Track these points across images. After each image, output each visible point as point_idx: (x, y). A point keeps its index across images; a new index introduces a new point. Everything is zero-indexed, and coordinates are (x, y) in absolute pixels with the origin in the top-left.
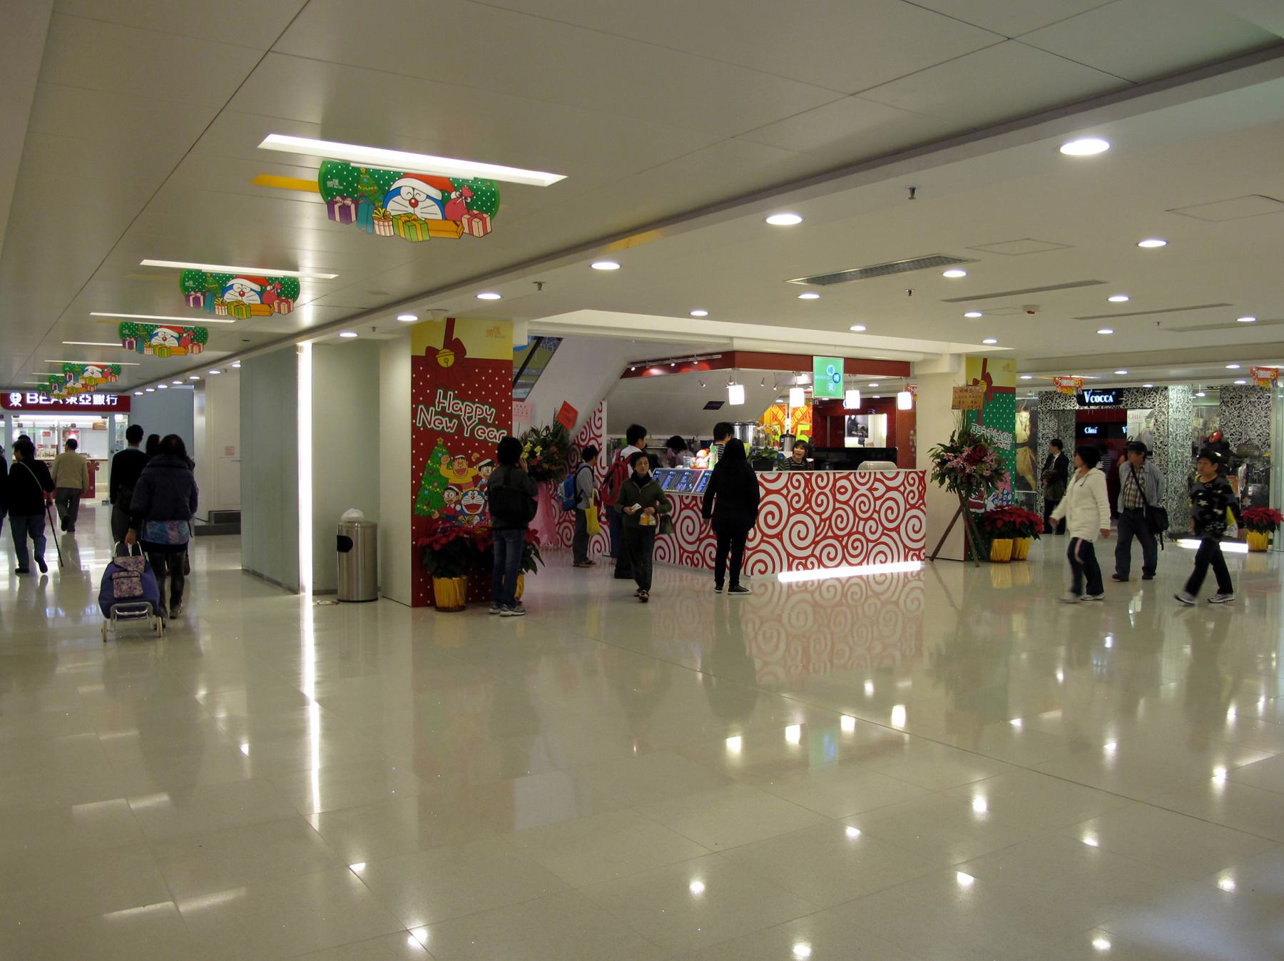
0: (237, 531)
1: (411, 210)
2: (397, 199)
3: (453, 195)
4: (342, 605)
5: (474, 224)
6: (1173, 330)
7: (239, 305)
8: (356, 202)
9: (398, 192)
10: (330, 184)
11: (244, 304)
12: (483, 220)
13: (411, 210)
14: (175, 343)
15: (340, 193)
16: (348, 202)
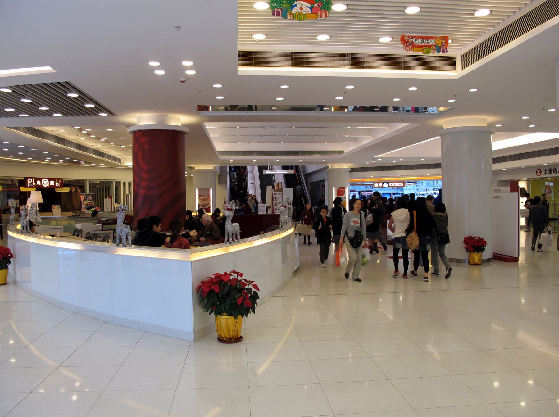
0: (493, 159)
1: (300, 11)
2: (296, 8)
3: (315, 5)
4: (240, 272)
5: (322, 14)
6: (250, 108)
7: (300, 14)
8: (282, 10)
9: (296, 5)
10: (273, 5)
11: (302, 14)
12: (326, 13)
13: (300, 11)
14: (309, 11)
15: (276, 7)
16: (279, 10)
